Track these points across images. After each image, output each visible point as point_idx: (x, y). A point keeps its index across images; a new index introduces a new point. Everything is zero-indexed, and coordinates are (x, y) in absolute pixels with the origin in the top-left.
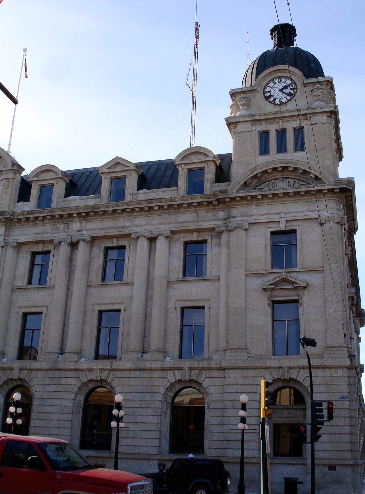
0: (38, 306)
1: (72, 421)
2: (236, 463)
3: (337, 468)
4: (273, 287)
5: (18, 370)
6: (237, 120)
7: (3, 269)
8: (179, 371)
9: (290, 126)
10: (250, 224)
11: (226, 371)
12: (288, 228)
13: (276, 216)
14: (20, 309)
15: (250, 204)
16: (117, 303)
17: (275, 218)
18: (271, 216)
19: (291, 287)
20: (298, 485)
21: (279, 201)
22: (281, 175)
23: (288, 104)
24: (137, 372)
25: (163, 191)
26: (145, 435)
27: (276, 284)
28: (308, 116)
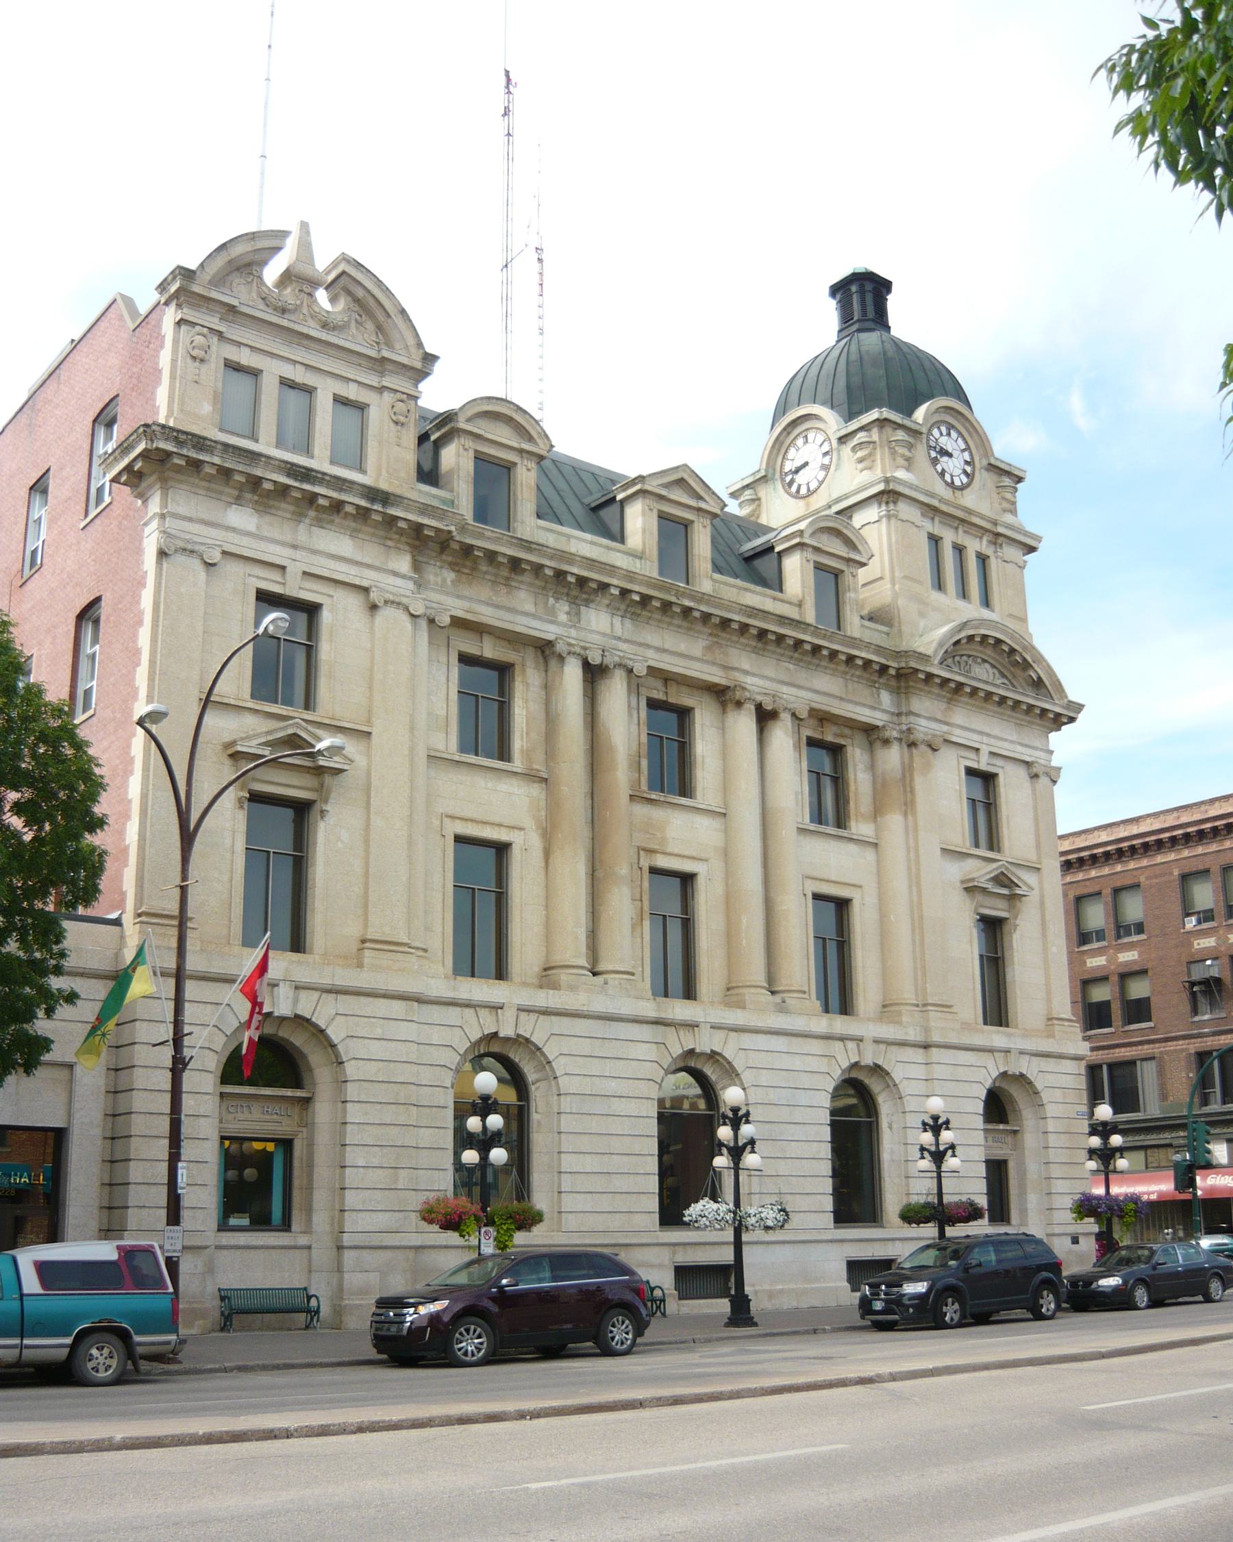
0: (500, 825)
1: (560, 1153)
2: (727, 1243)
5: (514, 1012)
6: (906, 491)
9: (974, 546)
10: (224, 553)
13: (975, 737)
14: (447, 821)
15: (215, 491)
16: (693, 858)
17: (276, 554)
18: (263, 546)
19: (1005, 891)
21: (982, 708)
22: (981, 652)
25: (774, 599)
28: (1001, 540)
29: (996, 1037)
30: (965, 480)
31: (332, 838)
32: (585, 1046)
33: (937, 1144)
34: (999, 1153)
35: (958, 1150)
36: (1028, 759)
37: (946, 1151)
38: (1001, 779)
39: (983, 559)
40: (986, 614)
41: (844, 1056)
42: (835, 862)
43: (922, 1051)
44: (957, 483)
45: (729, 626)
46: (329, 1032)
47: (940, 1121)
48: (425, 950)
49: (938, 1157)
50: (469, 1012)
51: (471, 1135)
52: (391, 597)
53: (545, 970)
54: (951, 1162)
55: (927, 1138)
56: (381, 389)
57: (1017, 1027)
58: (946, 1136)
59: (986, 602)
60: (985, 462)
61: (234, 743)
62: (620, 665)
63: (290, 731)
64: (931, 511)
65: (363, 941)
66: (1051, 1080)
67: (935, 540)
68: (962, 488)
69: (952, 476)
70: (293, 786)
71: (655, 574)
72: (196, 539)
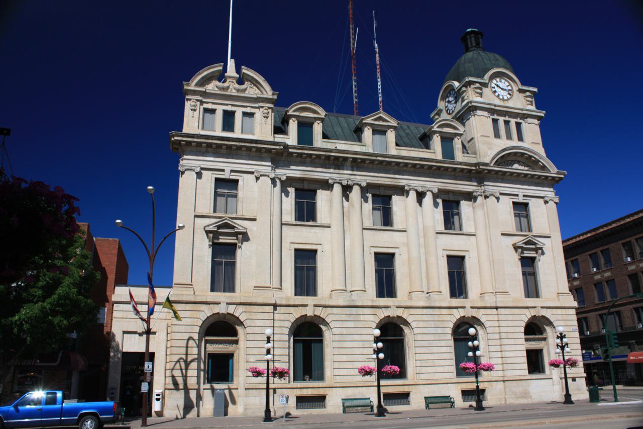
3: (577, 379)
4: (216, 229)
7: (485, 215)
8: (462, 309)
11: (499, 309)
12: (232, 177)
19: (533, 247)
20: (599, 391)
23: (509, 101)
24: (428, 310)
26: (442, 363)
27: (219, 227)
29: (531, 302)
30: (509, 96)
31: (244, 255)
32: (344, 317)
33: (562, 344)
34: (534, 345)
35: (569, 345)
36: (542, 195)
37: (565, 345)
38: (530, 205)
39: (518, 125)
40: (520, 144)
41: (458, 314)
42: (455, 244)
43: (495, 310)
44: (505, 98)
45: (191, 145)
46: (240, 318)
47: (563, 335)
48: (441, 292)
49: (562, 348)
50: (527, 310)
51: (470, 347)
52: (263, 173)
53: (409, 293)
54: (567, 349)
55: (559, 341)
56: (259, 108)
57: (542, 298)
58: (565, 340)
59: (520, 138)
60: (517, 89)
61: (516, 244)
62: (430, 191)
63: (529, 239)
64: (492, 111)
65: (558, 294)
66: (556, 317)
67: (495, 121)
68: (508, 99)
69: (503, 96)
70: (532, 254)
71: (297, 145)
72: (191, 165)
